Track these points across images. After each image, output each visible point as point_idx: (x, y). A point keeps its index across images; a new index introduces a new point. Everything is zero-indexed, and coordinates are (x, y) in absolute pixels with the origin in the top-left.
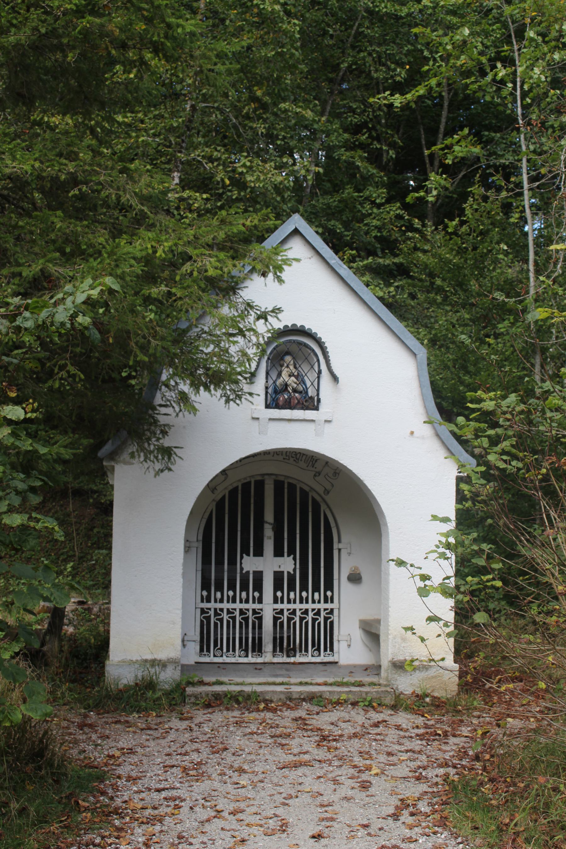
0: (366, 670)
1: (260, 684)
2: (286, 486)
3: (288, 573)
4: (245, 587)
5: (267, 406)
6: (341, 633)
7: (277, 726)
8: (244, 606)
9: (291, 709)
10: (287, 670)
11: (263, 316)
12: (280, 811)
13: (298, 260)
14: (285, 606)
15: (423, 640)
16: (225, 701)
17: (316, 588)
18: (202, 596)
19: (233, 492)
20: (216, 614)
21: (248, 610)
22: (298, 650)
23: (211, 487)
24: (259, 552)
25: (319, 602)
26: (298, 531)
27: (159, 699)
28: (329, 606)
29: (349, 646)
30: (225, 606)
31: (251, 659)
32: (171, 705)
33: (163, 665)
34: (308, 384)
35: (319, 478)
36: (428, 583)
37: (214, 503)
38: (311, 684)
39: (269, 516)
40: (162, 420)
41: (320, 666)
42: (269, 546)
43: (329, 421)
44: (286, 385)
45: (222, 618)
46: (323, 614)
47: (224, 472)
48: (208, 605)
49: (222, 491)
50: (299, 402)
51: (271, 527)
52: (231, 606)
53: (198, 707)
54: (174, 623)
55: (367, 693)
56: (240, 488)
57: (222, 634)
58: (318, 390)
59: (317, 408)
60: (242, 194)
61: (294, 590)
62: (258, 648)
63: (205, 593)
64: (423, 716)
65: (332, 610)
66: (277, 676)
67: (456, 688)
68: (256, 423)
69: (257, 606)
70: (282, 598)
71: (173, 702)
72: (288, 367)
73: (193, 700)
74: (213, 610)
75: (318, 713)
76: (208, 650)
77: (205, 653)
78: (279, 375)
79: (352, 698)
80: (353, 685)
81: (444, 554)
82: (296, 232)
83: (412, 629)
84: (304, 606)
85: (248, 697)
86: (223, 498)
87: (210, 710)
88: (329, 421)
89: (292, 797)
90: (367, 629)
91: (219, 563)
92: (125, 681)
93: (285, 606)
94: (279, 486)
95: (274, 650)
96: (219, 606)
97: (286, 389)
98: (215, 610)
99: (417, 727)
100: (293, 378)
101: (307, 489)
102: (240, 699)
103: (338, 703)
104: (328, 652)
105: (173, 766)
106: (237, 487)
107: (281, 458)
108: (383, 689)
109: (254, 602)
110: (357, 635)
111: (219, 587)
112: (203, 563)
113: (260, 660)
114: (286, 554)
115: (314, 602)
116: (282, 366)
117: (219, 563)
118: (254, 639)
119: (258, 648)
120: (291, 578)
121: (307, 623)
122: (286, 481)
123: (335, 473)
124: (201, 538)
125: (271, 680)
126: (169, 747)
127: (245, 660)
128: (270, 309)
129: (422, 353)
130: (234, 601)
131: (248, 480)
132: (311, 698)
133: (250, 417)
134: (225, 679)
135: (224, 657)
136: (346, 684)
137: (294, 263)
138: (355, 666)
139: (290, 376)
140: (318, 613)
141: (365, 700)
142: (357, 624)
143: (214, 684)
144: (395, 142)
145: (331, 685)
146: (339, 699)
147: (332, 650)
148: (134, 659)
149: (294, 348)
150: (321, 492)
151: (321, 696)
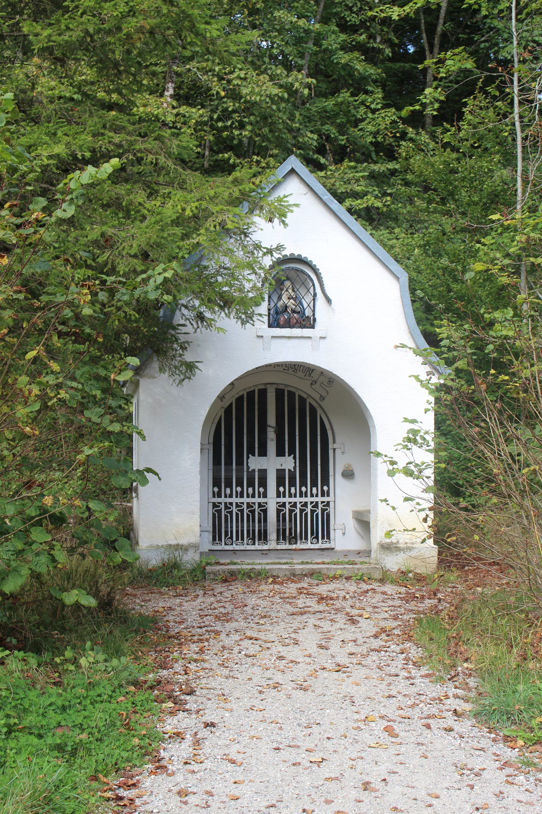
0: (359, 553)
1: (268, 564)
2: (286, 393)
3: (289, 470)
4: (251, 484)
5: (270, 326)
6: (337, 523)
7: (285, 593)
8: (251, 500)
9: (295, 582)
10: (289, 554)
11: (270, 252)
12: (293, 635)
13: (297, 205)
14: (287, 500)
15: (394, 508)
16: (240, 577)
17: (314, 484)
18: (214, 492)
19: (239, 400)
20: (226, 507)
21: (254, 503)
22: (298, 538)
23: (221, 397)
24: (263, 453)
25: (317, 496)
26: (297, 434)
27: (183, 576)
28: (325, 499)
29: (344, 534)
30: (234, 500)
31: (257, 547)
32: (194, 581)
33: (184, 549)
34: (305, 305)
35: (316, 386)
36: (395, 466)
37: (223, 410)
38: (311, 563)
39: (271, 420)
40: (182, 338)
41: (319, 551)
42: (272, 447)
43: (324, 338)
44: (286, 307)
45: (232, 511)
46: (320, 506)
47: (232, 384)
48: (219, 500)
49: (230, 399)
50: (297, 321)
51: (273, 430)
52: (239, 500)
53: (216, 582)
54: (193, 514)
55: (358, 569)
56: (245, 396)
57: (232, 527)
58: (314, 311)
59: (313, 327)
60: (237, 105)
61: (295, 486)
62: (264, 537)
63: (216, 489)
64: (406, 587)
65: (328, 503)
66: (281, 558)
67: (435, 566)
68: (260, 340)
69: (262, 500)
70: (284, 492)
71: (196, 579)
72: (287, 291)
73: (212, 576)
74: (223, 504)
75: (317, 585)
76: (220, 539)
77: (217, 542)
78: (280, 298)
79: (346, 574)
80: (347, 563)
81: (407, 446)
82: (292, 171)
83: (386, 500)
84: (304, 500)
85: (259, 573)
86: (231, 405)
87: (227, 584)
88: (324, 338)
89: (300, 629)
90: (359, 518)
91: (229, 463)
92: (154, 562)
93: (287, 500)
94: (280, 393)
95: (278, 539)
96: (229, 500)
97: (286, 309)
98: (226, 503)
99: (400, 593)
100: (292, 301)
101: (305, 396)
102: (252, 575)
103: (335, 578)
104: (326, 540)
105: (207, 615)
106: (243, 395)
107: (281, 369)
108: (372, 566)
109: (259, 497)
110: (351, 525)
111: (229, 484)
112: (214, 464)
113: (265, 547)
114: (287, 454)
115: (312, 496)
116: (282, 290)
117: (229, 463)
118: (260, 531)
119: (264, 537)
120: (292, 475)
121: (306, 514)
122: (286, 390)
123: (330, 381)
124: (211, 441)
125: (277, 561)
126: (201, 605)
127: (252, 547)
128: (275, 246)
129: (405, 277)
130: (242, 496)
131: (252, 389)
132: (311, 574)
133: (255, 336)
134: (238, 561)
135: (234, 545)
136: (342, 563)
137: (294, 209)
138: (349, 551)
139: (289, 298)
140: (316, 505)
141: (357, 575)
142: (351, 515)
143: (229, 564)
144: (390, 39)
145: (328, 564)
146: (335, 575)
147: (329, 537)
148: (160, 545)
149: (292, 274)
150: (317, 398)
151: (320, 573)
